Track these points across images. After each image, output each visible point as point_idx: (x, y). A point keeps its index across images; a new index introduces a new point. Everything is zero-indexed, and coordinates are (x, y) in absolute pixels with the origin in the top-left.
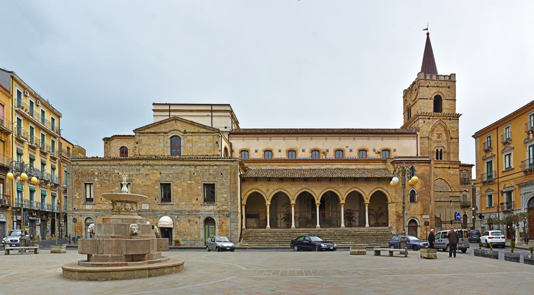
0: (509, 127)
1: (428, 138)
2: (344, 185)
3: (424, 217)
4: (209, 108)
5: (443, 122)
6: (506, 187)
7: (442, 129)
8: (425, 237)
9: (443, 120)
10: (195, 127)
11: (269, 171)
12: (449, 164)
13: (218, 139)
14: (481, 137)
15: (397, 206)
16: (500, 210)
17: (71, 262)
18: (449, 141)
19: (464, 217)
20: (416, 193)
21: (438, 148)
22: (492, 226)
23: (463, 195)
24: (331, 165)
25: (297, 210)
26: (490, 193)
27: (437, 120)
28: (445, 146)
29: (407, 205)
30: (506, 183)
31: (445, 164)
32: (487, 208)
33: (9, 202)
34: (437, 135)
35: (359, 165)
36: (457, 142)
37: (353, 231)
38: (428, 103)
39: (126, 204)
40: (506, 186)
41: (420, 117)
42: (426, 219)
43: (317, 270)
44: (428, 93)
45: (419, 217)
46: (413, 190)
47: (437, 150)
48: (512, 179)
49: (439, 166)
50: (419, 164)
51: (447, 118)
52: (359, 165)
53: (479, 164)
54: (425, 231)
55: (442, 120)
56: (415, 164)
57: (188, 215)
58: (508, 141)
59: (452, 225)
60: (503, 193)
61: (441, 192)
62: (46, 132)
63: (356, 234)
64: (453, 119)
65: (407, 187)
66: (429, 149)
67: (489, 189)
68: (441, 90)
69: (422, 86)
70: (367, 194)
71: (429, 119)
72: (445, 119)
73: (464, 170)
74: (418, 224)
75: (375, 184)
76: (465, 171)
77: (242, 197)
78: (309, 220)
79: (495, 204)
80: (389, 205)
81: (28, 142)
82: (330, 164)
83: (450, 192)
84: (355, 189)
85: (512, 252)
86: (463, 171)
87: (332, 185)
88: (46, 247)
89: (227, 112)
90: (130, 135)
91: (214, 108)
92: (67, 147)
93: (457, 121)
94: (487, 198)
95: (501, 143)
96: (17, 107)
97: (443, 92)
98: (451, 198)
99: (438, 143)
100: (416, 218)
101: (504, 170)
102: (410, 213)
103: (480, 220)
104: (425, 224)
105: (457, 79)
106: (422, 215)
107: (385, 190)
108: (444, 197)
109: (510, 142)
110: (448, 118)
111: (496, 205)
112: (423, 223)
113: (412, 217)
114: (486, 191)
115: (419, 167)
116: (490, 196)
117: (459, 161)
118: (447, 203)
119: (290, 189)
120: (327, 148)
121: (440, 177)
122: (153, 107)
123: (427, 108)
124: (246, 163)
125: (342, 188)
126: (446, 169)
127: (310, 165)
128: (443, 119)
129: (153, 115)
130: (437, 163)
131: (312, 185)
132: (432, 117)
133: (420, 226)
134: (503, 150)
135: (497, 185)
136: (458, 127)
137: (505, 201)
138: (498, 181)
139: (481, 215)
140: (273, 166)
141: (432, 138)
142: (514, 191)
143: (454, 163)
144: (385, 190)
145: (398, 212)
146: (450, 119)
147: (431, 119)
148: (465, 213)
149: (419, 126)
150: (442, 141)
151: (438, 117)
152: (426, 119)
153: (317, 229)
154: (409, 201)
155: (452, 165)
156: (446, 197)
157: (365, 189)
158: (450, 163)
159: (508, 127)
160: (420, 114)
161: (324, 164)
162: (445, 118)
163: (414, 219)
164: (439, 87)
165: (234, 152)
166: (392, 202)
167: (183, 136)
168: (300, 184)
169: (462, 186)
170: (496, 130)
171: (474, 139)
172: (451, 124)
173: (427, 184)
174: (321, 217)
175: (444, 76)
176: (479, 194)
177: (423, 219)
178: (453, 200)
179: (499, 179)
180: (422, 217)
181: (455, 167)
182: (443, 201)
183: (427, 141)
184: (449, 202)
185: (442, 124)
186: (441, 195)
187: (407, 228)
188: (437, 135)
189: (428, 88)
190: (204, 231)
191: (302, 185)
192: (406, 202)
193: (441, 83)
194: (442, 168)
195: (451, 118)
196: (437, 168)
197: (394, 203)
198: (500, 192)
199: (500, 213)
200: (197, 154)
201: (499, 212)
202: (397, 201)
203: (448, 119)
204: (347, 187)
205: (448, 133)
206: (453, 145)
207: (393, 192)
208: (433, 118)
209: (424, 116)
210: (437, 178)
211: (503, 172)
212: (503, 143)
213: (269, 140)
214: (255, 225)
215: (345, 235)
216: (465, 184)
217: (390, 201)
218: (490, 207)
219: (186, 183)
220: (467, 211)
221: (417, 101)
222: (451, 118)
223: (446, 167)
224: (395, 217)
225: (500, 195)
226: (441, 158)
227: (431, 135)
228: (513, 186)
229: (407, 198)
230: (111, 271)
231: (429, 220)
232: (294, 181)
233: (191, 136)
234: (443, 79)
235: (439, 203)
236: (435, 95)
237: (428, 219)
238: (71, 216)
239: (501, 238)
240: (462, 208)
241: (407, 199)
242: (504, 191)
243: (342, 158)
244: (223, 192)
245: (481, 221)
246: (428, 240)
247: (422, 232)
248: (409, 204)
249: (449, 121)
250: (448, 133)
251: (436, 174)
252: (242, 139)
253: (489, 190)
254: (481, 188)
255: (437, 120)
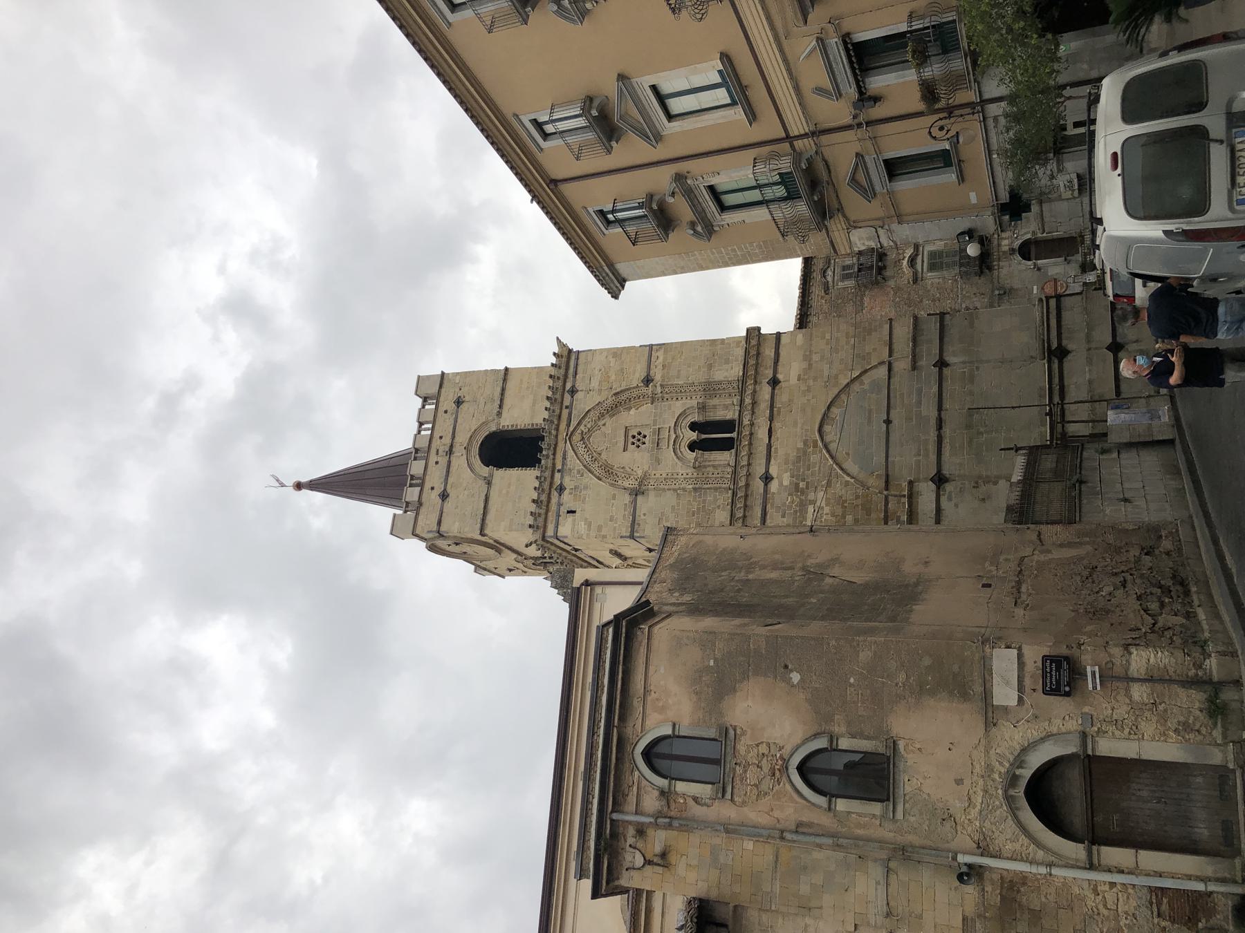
0: (654, 88)
1: (637, 493)
3: (1005, 695)
5: (579, 424)
7: (607, 430)
8: (1182, 693)
9: (574, 423)
12: (756, 382)
14: (613, 256)
16: (970, 96)
18: (659, 389)
19: (1033, 255)
20: (822, 743)
21: (685, 443)
22: (1070, 126)
23: (933, 267)
26: (877, 175)
27: (570, 453)
28: (678, 407)
30: (807, 85)
31: (754, 403)
32: (962, 178)
34: (631, 447)
36: (666, 352)
38: (504, 492)
40: (826, 83)
41: (550, 532)
42: (1028, 682)
43: (1016, 912)
44: (466, 492)
45: (1011, 737)
46: (801, 768)
47: (692, 447)
48: (781, 50)
49: (762, 434)
50: (635, 702)
51: (567, 407)
53: (734, 250)
54: (1128, 694)
55: (571, 429)
56: (629, 731)
58: (803, 170)
59: (1070, 347)
60: (866, 99)
61: (888, 422)
64: (574, 381)
65: (777, 814)
66: (684, 489)
67: (853, 180)
68: (462, 438)
69: (439, 523)
71: (561, 489)
72: (570, 414)
73: (825, 277)
74: (1071, 749)
76: (830, 273)
78: (987, 238)
79: (935, 132)
83: (890, 370)
86: (829, 279)
90: (1188, 43)
93: (582, 356)
94: (906, 186)
95: (609, 151)
96: (1240, 882)
97: (622, 388)
98: (922, 363)
99: (664, 444)
100: (1019, 762)
101: (738, 113)
103: (1035, 208)
104: (1067, 694)
105: (613, 299)
106: (991, 715)
108: (919, 403)
109: (596, 104)
110: (567, 397)
111: (941, 129)
112: (1060, 706)
113: (1010, 800)
114: (868, 193)
116: (894, 168)
117: (744, 334)
118: (947, 385)
120: (547, 378)
121: (817, 428)
122: (961, 185)
123: (520, 496)
126: (777, 399)
128: (568, 425)
130: (750, 444)
132: (558, 476)
133: (1084, 735)
134: (645, 136)
135: (824, 139)
136: (605, 354)
137: (910, 76)
138: (805, 135)
139: (1003, 208)
141: (640, 473)
142: (847, 26)
143: (752, 362)
146: (573, 392)
147: (562, 477)
148: (1012, 251)
150: (655, 422)
151: (561, 445)
152: (560, 505)
154: (876, 808)
155: (761, 369)
156: (920, 391)
158: (750, 382)
159: (661, 98)
160: (538, 536)
162: (565, 412)
163: (1023, 784)
164: (451, 446)
169: (893, 277)
170: (566, 189)
171: (628, 284)
172: (593, 385)
174: (1187, 63)
175: (421, 424)
176: (889, 230)
177: (1020, 700)
178: (936, 351)
179: (794, 131)
180: (1006, 709)
181: (772, 354)
182: (940, 409)
183: (652, 496)
184: (946, 371)
185: (589, 426)
186: (909, 419)
188: (631, 447)
189: (448, 496)
193: (441, 437)
194: (771, 419)
195: (568, 386)
196: (769, 446)
198: (861, 119)
199: (986, 96)
201: (984, 102)
203: (572, 403)
205: (623, 397)
206: (966, 821)
208: (559, 471)
209: (550, 514)
210: (820, 443)
211: (752, 115)
212: (610, 140)
214: (1215, 895)
216: (884, 267)
218: (954, 161)
219: (1174, 661)
220: (1005, 242)
221: (495, 541)
222: (568, 386)
223: (767, 397)
225: (878, 112)
226: (728, 426)
227: (628, 476)
228: (820, 40)
229: (859, 826)
231: (1034, 654)
235: (947, 431)
236: (477, 462)
237: (1020, 656)
238: (1187, 508)
240: (990, 268)
241: (864, 826)
242: (851, 91)
245: (1041, 203)
248: (899, 815)
249: (579, 396)
250: (623, 397)
251: (798, 449)
253: (861, 177)
254: (852, 225)
255: (570, 453)
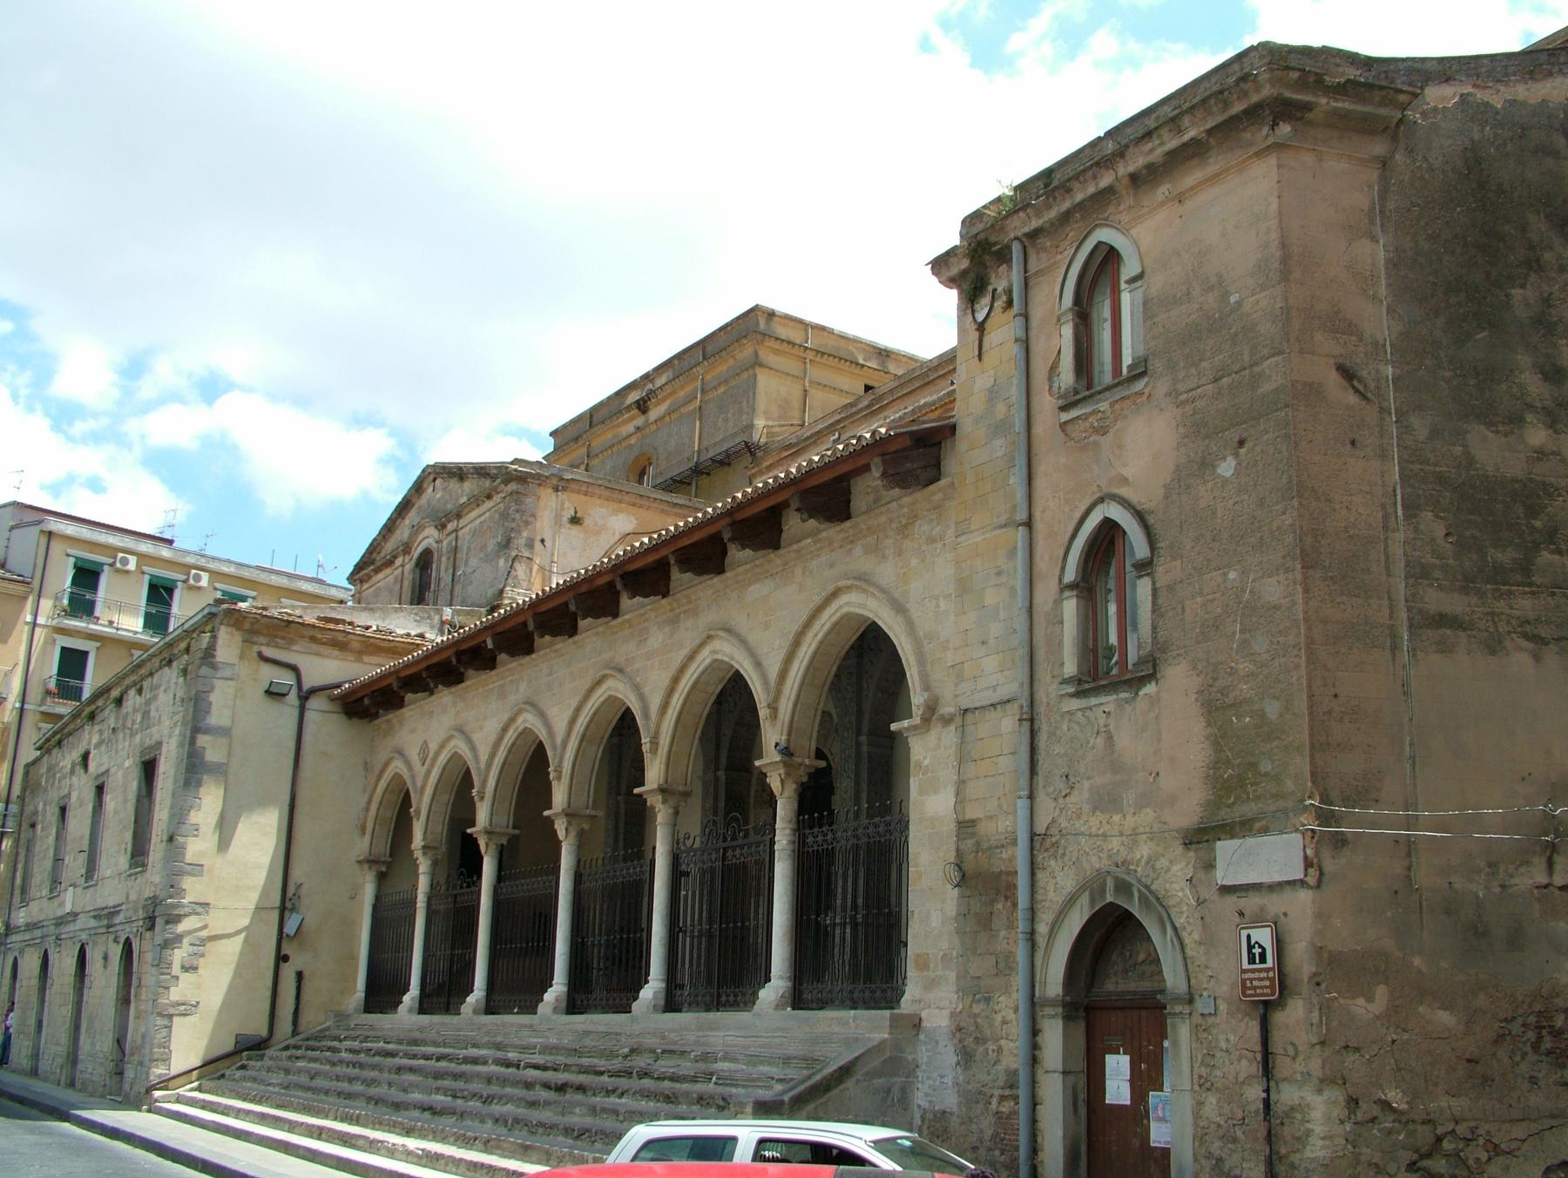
6: (454, 535)
33: (1405, 429)
39: (1536, 860)
81: (1399, 1133)
88: (771, 1114)
92: (356, 864)
106: (1201, 837)
127: (807, 625)
149: (1464, 584)
165: (1017, 340)
173: (1266, 387)
180: (1210, 866)
230: (1032, 895)
243: (1269, 929)
247: (1212, 1099)
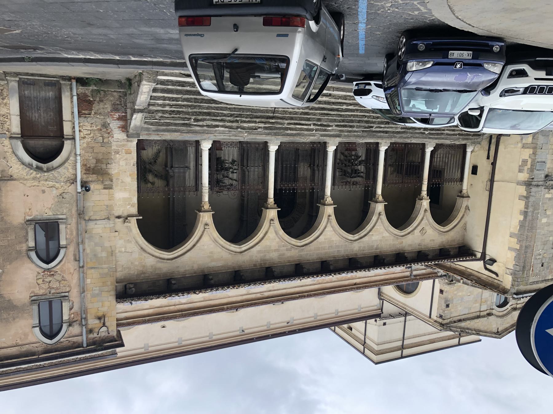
2: (267, 257)
4: (406, 352)
10: (473, 328)
11: (242, 78)
13: (446, 312)
15: (107, 206)
17: (420, 111)
24: (250, 292)
25: (191, 195)
29: (70, 210)
35: (185, 304)
37: (259, 130)
52: (185, 304)
57: (403, 348)
62: (371, 287)
63: (258, 120)
65: (72, 271)
70: (271, 234)
75: (182, 270)
77: (74, 150)
80: (134, 210)
82: (253, 296)
84: (238, 250)
85: (511, 233)
87: (165, 267)
89: (380, 350)
91: (398, 354)
100: (30, 166)
102: (57, 185)
107: (149, 253)
115: (27, 341)
119: (383, 237)
124: (407, 277)
125: (273, 248)
127: (296, 287)
129: (469, 197)
131: (338, 251)
140: (318, 283)
144: (149, 253)
145: (105, 188)
153: (338, 140)
157: (211, 253)
161: (266, 294)
163: (40, 164)
166: (126, 218)
167: (492, 309)
168: (363, 251)
187: (65, 132)
190: (33, 232)
191: (360, 247)
192: (73, 221)
197: (119, 217)
200: (545, 278)
202: (109, 224)
204: (259, 252)
207: (123, 249)
213: (319, 314)
215: (286, 122)
217: (134, 221)
224: (114, 169)
232: (419, 252)
233: (482, 311)
234: (277, 78)
239: (312, 125)
244: (546, 228)
246: (411, 106)
252: (400, 88)
